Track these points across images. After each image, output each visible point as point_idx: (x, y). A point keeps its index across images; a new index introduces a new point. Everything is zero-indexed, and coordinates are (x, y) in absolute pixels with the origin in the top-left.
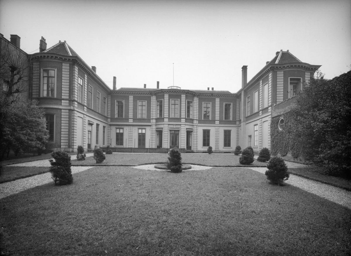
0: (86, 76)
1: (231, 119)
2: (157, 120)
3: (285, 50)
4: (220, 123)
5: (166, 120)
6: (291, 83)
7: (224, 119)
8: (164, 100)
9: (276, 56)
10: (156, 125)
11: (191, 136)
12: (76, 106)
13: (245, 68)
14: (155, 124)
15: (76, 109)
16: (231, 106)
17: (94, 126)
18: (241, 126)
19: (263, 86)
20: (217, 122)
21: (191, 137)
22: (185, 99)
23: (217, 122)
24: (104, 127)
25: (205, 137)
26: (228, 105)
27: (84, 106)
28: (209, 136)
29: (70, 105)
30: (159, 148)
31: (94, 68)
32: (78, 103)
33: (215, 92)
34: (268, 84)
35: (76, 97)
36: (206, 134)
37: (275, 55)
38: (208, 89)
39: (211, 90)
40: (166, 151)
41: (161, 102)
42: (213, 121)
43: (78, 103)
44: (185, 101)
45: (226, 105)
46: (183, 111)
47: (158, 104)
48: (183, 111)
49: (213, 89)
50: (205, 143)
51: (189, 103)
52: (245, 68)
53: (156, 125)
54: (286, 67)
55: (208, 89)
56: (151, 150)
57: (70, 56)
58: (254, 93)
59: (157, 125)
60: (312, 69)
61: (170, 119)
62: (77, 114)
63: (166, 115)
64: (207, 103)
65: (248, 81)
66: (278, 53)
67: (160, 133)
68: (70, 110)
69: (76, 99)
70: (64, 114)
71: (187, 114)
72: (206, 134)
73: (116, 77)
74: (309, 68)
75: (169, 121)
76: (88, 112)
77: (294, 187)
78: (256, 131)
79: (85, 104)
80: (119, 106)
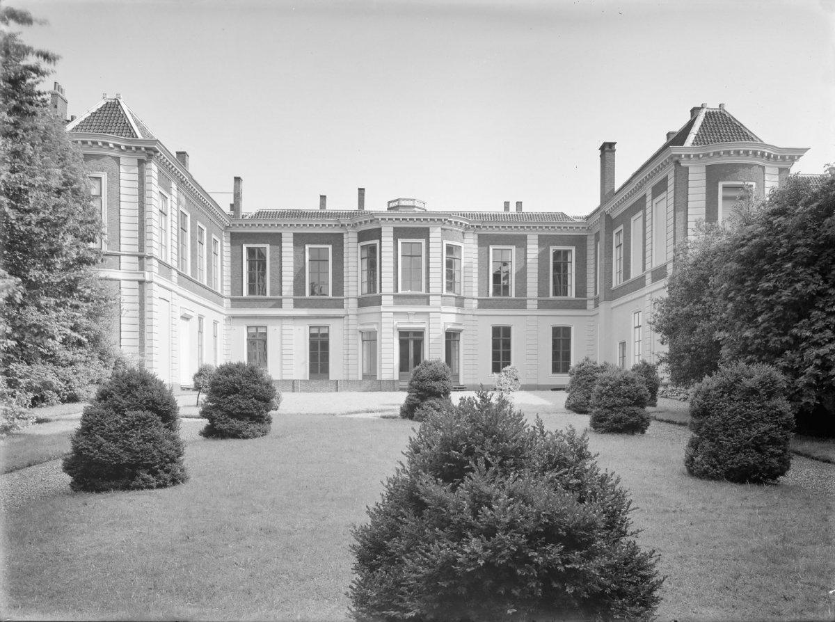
0: (174, 186)
1: (572, 293)
2: (362, 303)
3: (713, 105)
4: (540, 307)
5: (387, 301)
6: (725, 198)
7: (551, 296)
8: (381, 244)
9: (666, 141)
10: (357, 315)
11: (457, 345)
12: (156, 269)
13: (607, 149)
14: (355, 312)
15: (155, 279)
16: (572, 257)
17: (195, 320)
18: (598, 314)
19: (654, 204)
20: (532, 304)
21: (457, 348)
22: (440, 240)
23: (532, 304)
24: (215, 323)
25: (499, 348)
26: (562, 253)
27: (170, 268)
28: (507, 345)
29: (142, 268)
30: (371, 381)
31: (182, 155)
32: (160, 262)
33: (531, 216)
34: (665, 200)
35: (154, 249)
36: (502, 339)
37: (688, 118)
38: (507, 204)
39: (513, 209)
40: (391, 386)
41: (372, 249)
42: (521, 304)
43: (160, 262)
44: (440, 245)
45: (557, 254)
46: (436, 270)
47: (365, 255)
48: (436, 270)
49: (519, 204)
50: (322, 361)
51: (450, 249)
52: (607, 149)
53: (357, 315)
54: (711, 154)
55: (507, 204)
56: (350, 384)
57: (141, 141)
58: (632, 222)
59: (360, 314)
60: (783, 158)
61: (399, 299)
62: (155, 292)
63: (387, 285)
64: (502, 250)
65: (620, 179)
66: (695, 112)
67: (370, 339)
68: (141, 282)
69: (156, 253)
70: (128, 294)
71: (447, 283)
72: (502, 339)
73: (242, 177)
74: (775, 157)
75: (396, 304)
76: (179, 283)
77: (616, 433)
78: (639, 327)
79: (175, 264)
80: (251, 267)
